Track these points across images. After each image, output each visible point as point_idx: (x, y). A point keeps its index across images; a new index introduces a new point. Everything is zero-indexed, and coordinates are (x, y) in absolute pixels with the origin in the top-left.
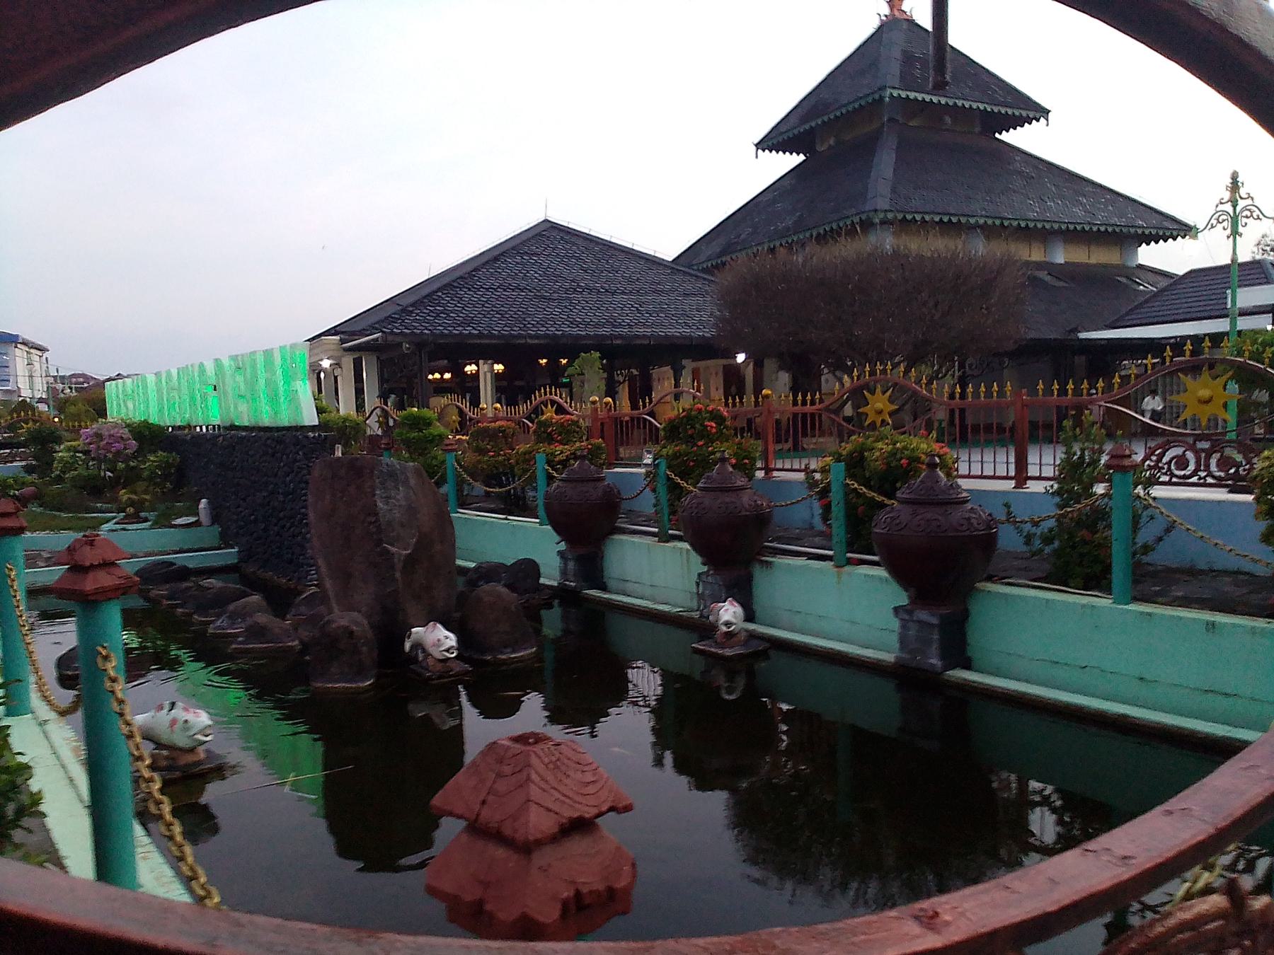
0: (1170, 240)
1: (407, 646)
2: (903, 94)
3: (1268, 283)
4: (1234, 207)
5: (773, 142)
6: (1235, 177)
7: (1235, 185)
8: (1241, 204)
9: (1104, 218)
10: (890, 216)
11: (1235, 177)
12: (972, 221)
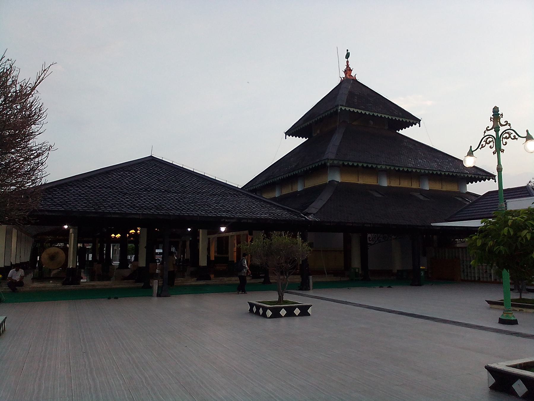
0: (482, 181)
1: (506, 274)
2: (347, 109)
3: (530, 196)
4: (497, 131)
5: (293, 132)
6: (496, 111)
7: (496, 115)
8: (502, 129)
9: (447, 168)
10: (336, 162)
11: (496, 111)
12: (379, 167)
